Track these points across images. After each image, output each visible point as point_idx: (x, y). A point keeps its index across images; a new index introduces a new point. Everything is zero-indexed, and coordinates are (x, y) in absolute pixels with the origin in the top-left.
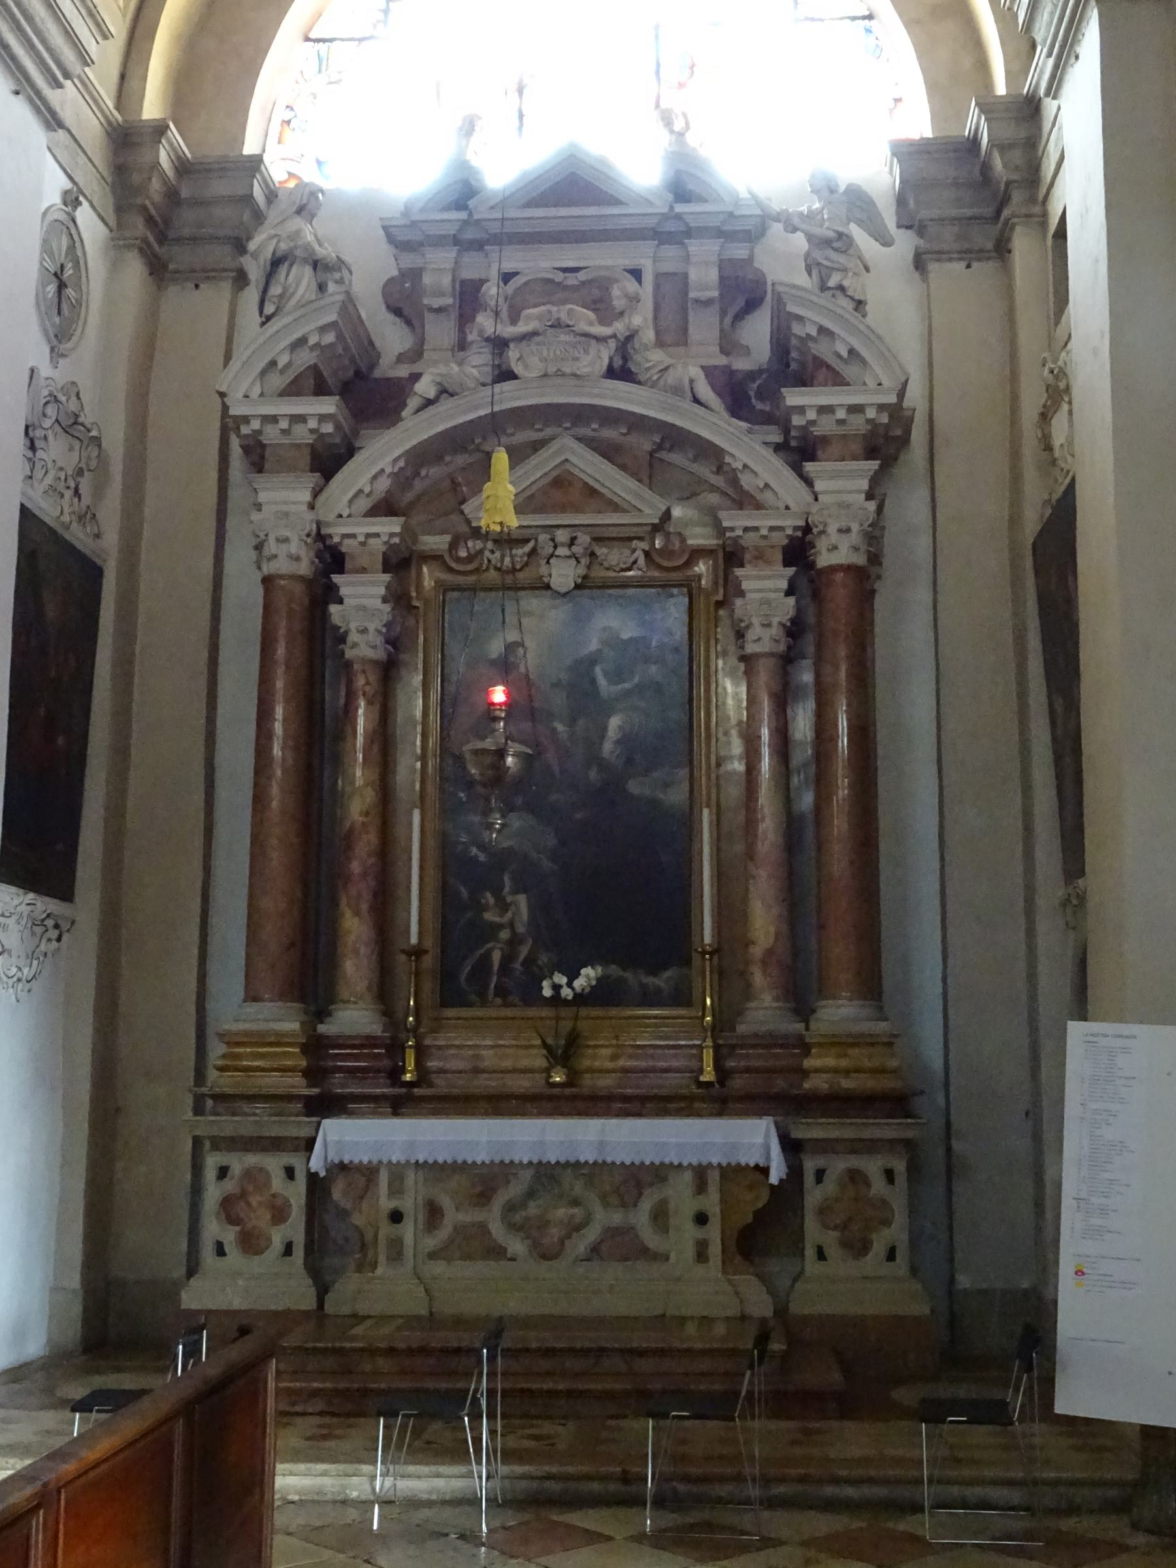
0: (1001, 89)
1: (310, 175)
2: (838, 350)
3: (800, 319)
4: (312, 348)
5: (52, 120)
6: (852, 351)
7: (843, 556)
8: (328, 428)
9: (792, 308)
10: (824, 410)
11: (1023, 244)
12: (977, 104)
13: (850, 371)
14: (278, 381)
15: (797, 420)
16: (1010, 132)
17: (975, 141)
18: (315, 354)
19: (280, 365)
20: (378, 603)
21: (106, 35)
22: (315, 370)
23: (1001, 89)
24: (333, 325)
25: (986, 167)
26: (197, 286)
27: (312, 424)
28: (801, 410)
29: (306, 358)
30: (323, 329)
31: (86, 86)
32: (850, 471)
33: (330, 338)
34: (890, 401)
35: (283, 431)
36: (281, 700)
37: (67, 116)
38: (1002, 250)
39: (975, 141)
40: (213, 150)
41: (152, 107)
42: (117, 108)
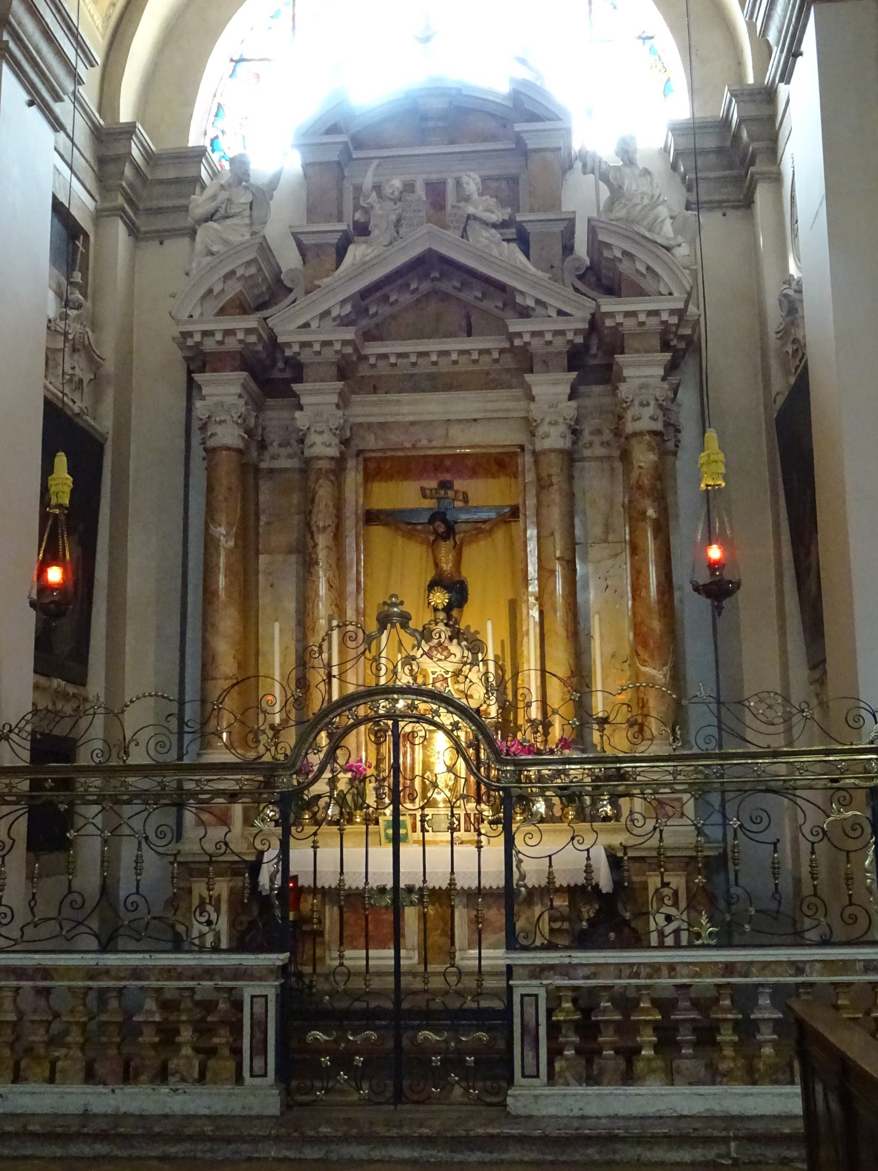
0: (751, 80)
1: (378, 884)
2: (638, 267)
3: (609, 246)
4: (239, 279)
5: (56, 124)
6: (648, 268)
7: (645, 424)
8: (253, 339)
9: (602, 237)
10: (628, 314)
11: (762, 194)
12: (729, 90)
13: (648, 284)
14: (215, 305)
15: (609, 323)
16: (753, 110)
17: (726, 121)
18: (240, 284)
19: (215, 292)
20: (234, 399)
21: (92, 63)
22: (239, 296)
23: (751, 80)
24: (254, 261)
25: (737, 137)
26: (161, 243)
27: (240, 336)
28: (612, 315)
29: (234, 288)
30: (248, 264)
31: (76, 98)
32: (648, 361)
33: (253, 270)
34: (679, 307)
35: (218, 342)
36: (396, 408)
37: (67, 122)
38: (748, 203)
39: (727, 121)
40: (170, 144)
41: (125, 115)
42: (100, 112)
